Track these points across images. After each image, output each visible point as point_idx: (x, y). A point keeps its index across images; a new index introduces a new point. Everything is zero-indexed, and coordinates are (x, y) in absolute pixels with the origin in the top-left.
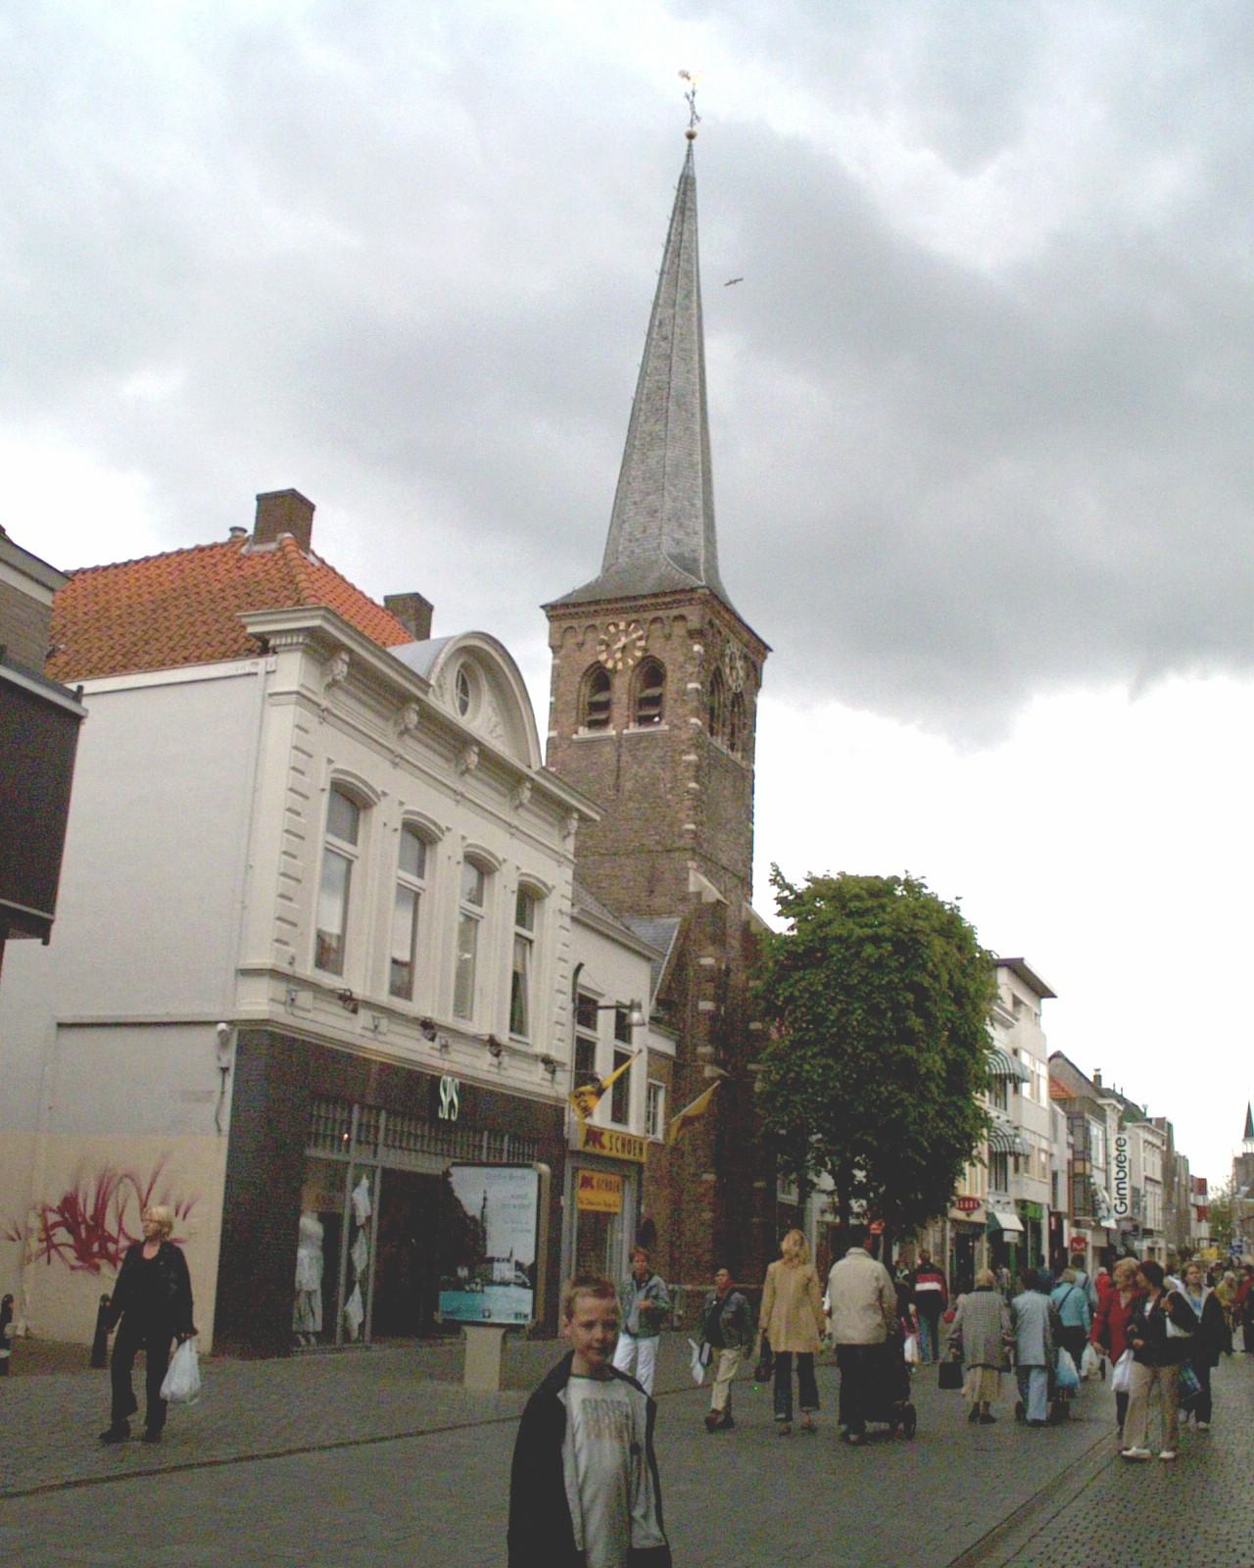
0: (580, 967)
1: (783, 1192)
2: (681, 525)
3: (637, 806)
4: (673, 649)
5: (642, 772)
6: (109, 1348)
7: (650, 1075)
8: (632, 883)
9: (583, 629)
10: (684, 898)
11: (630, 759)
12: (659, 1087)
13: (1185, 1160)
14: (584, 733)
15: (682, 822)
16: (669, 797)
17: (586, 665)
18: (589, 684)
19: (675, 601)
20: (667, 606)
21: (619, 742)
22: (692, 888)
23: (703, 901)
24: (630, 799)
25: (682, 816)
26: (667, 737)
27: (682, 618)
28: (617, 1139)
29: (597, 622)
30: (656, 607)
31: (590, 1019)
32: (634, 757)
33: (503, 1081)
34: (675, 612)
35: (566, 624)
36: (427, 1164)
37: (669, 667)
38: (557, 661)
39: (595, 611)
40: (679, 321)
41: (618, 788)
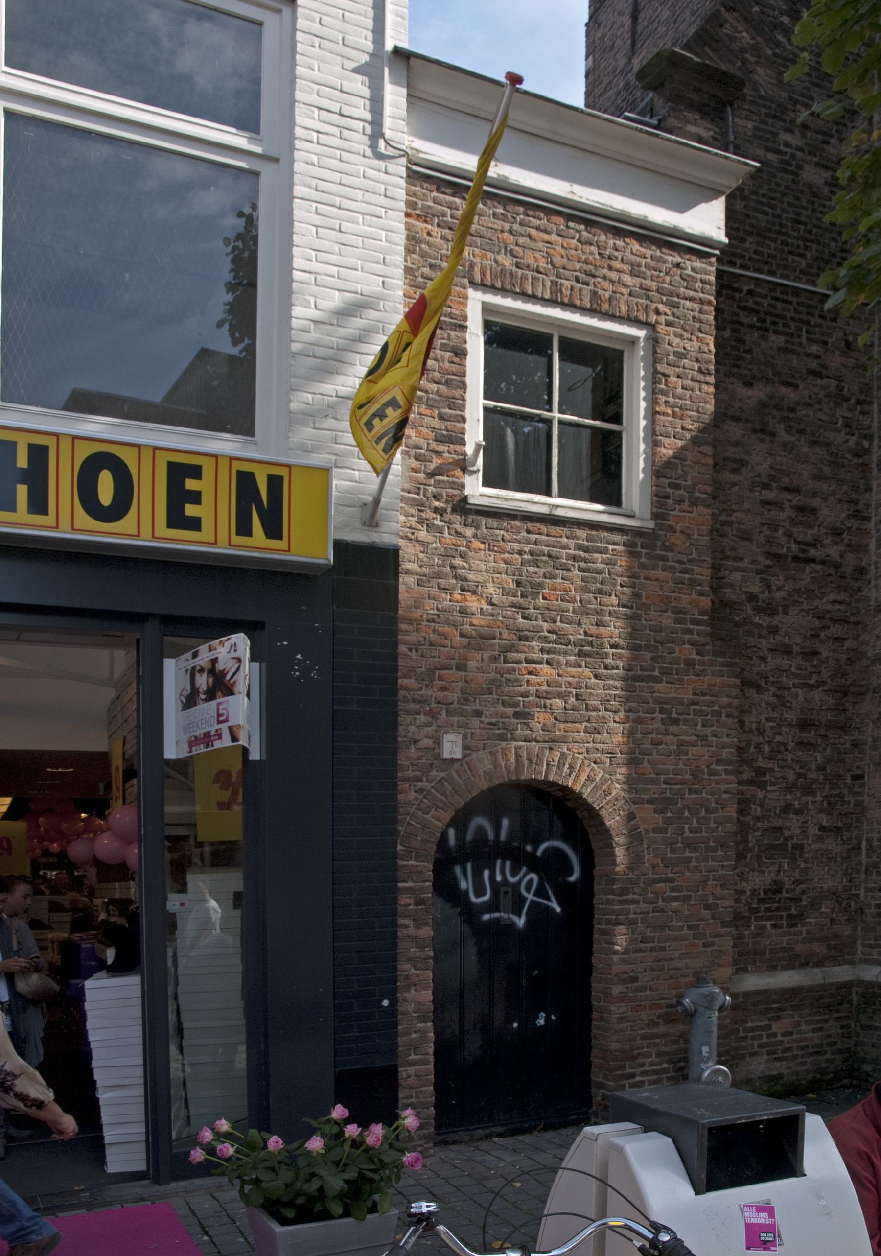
12: (633, 341)
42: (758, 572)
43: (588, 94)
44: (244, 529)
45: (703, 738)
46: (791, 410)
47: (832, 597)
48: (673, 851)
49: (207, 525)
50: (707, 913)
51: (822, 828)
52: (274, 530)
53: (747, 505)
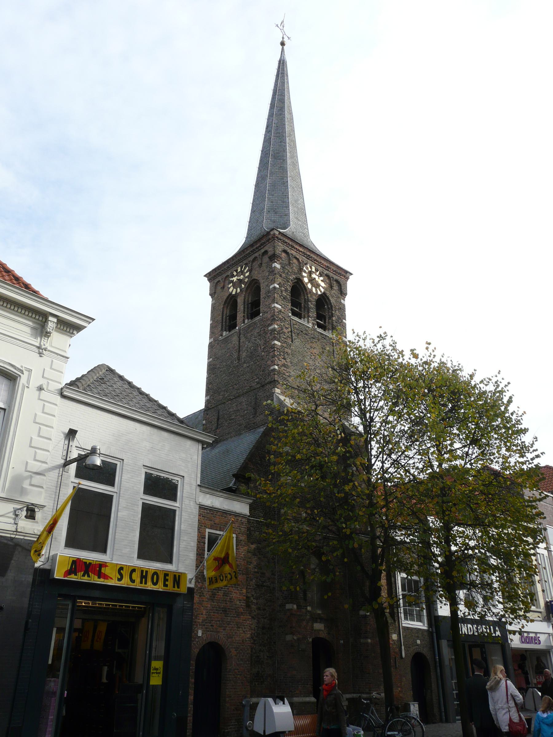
1: (406, 618)
3: (248, 365)
6: (189, 700)
8: (246, 412)
13: (149, 394)
15: (270, 366)
16: (263, 353)
17: (225, 297)
19: (262, 245)
20: (258, 249)
24: (245, 362)
32: (246, 338)
34: (263, 251)
37: (261, 281)
39: (228, 267)
41: (239, 359)
42: (254, 589)
43: (250, 511)
44: (174, 587)
45: (244, 632)
46: (260, 549)
47: (269, 595)
48: (238, 661)
49: (169, 586)
50: (245, 679)
51: (267, 657)
52: (178, 587)
53: (252, 573)
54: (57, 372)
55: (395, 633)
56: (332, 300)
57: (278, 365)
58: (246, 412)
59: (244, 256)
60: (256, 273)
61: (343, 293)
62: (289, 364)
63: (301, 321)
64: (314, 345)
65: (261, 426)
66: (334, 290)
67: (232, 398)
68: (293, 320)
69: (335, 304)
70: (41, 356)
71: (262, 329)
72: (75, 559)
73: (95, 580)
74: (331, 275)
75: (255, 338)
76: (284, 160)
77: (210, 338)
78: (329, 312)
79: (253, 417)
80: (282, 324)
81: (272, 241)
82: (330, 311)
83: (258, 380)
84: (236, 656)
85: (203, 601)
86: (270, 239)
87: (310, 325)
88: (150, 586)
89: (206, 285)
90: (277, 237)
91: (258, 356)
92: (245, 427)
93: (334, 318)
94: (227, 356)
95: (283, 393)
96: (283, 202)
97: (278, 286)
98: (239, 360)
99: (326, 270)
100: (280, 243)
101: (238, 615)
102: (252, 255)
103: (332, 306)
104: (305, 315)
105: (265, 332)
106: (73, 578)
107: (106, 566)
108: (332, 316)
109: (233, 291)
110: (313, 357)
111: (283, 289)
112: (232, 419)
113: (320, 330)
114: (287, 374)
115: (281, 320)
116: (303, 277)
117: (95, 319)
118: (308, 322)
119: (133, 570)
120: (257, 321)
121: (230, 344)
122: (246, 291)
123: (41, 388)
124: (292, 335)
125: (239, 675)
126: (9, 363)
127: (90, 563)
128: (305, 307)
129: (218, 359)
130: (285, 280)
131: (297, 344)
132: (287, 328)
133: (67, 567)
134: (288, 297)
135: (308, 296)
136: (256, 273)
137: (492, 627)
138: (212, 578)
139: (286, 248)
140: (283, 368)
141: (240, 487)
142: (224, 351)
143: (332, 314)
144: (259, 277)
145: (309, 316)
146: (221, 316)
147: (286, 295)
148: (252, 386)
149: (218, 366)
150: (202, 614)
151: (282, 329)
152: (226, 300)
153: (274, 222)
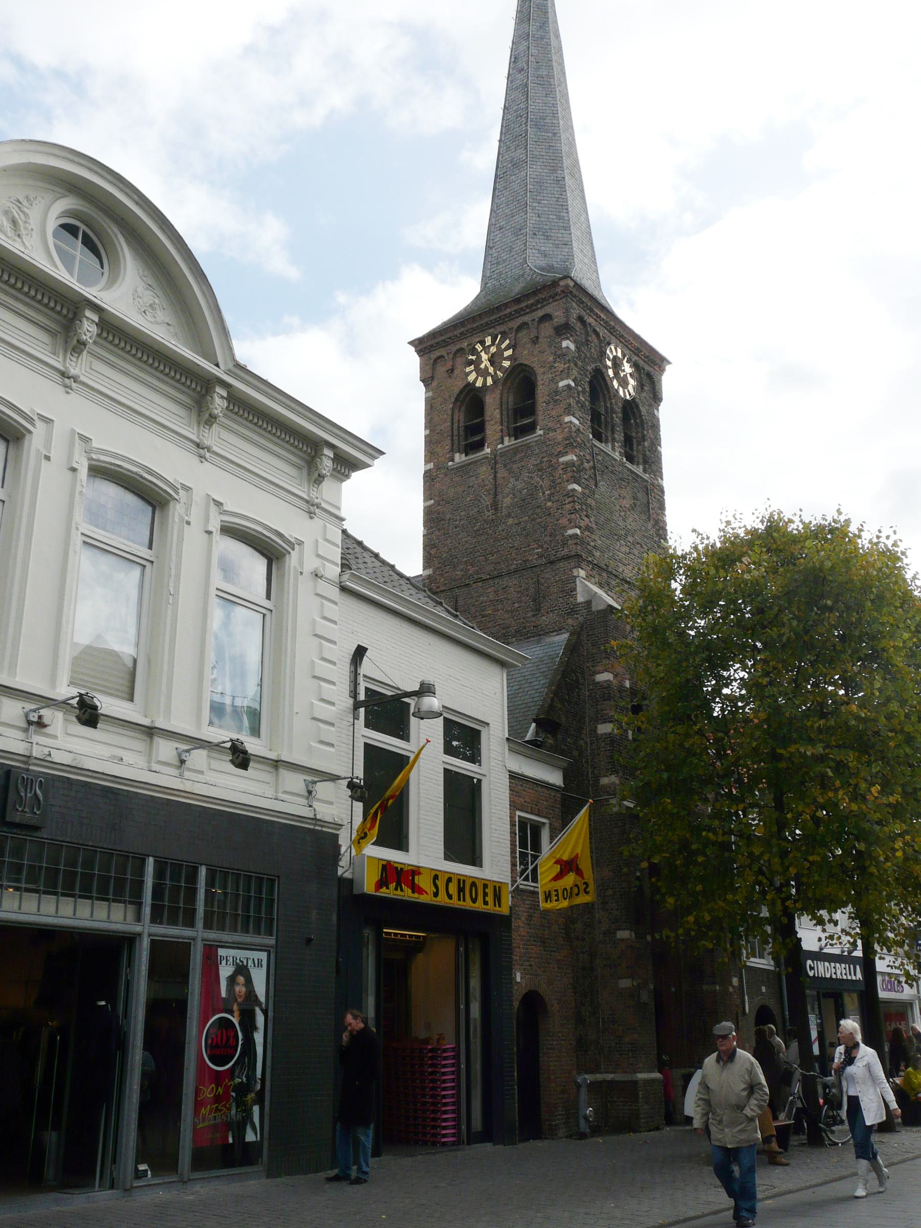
0: (360, 652)
2: (548, 238)
4: (542, 352)
5: (520, 485)
7: (514, 806)
8: (516, 605)
9: (451, 356)
10: (573, 610)
11: (506, 474)
12: (544, 824)
14: (459, 458)
15: (565, 528)
16: (549, 504)
17: (456, 391)
18: (463, 408)
19: (538, 302)
20: (532, 308)
21: (493, 461)
22: (580, 599)
23: (594, 609)
24: (509, 515)
25: (564, 521)
26: (541, 442)
27: (547, 317)
28: (485, 886)
29: (465, 345)
30: (520, 313)
31: (402, 730)
32: (510, 471)
33: (187, 786)
34: (540, 313)
35: (434, 355)
36: (51, 909)
37: (539, 371)
38: (430, 394)
39: (462, 334)
40: (533, 50)
41: (495, 506)
52: (500, 906)
54: (331, 546)
55: (736, 976)
56: (644, 410)
57: (580, 528)
58: (516, 605)
59: (500, 317)
60: (525, 352)
61: (656, 398)
62: (594, 526)
63: (601, 446)
64: (623, 492)
65: (552, 632)
66: (645, 391)
67: (484, 578)
68: (595, 446)
69: (647, 418)
70: (311, 518)
71: (546, 459)
72: (384, 863)
73: (407, 894)
74: (641, 363)
75: (529, 473)
76: (555, 134)
77: (427, 461)
78: (637, 433)
79: (534, 616)
80: (582, 454)
81: (561, 299)
82: (640, 430)
83: (540, 550)
84: (559, 1011)
85: (519, 926)
86: (556, 294)
87: (617, 456)
88: (468, 904)
89: (413, 361)
90: (571, 292)
91: (538, 507)
92: (516, 632)
93: (646, 444)
94: (469, 499)
95: (589, 577)
96: (560, 218)
97: (573, 384)
98: (496, 509)
99: (635, 354)
100: (574, 304)
101: (557, 949)
102: (518, 317)
103: (642, 421)
104: (607, 437)
105: (552, 466)
106: (384, 892)
107: (419, 873)
108: (644, 441)
109: (476, 379)
110: (623, 514)
111: (580, 388)
112: (488, 615)
113: (629, 465)
114: (592, 544)
115: (579, 445)
116: (607, 367)
117: (384, 453)
118: (613, 449)
119: (449, 880)
120: (534, 444)
121: (474, 478)
122: (504, 384)
123: (316, 575)
124: (595, 475)
125: (562, 1040)
126: (276, 531)
127: (402, 869)
128: (606, 422)
129: (448, 502)
130: (582, 373)
131: (603, 489)
132: (588, 462)
133: (376, 877)
134: (587, 403)
135: (611, 404)
136: (525, 352)
137: (852, 966)
138: (550, 891)
139: (583, 313)
140: (587, 533)
141: (546, 740)
142: (460, 489)
143: (644, 436)
144: (533, 362)
145: (614, 440)
146: (449, 424)
147: (583, 399)
148: (528, 560)
149: (448, 516)
150: (519, 947)
151: (582, 464)
152: (458, 395)
153: (545, 256)
